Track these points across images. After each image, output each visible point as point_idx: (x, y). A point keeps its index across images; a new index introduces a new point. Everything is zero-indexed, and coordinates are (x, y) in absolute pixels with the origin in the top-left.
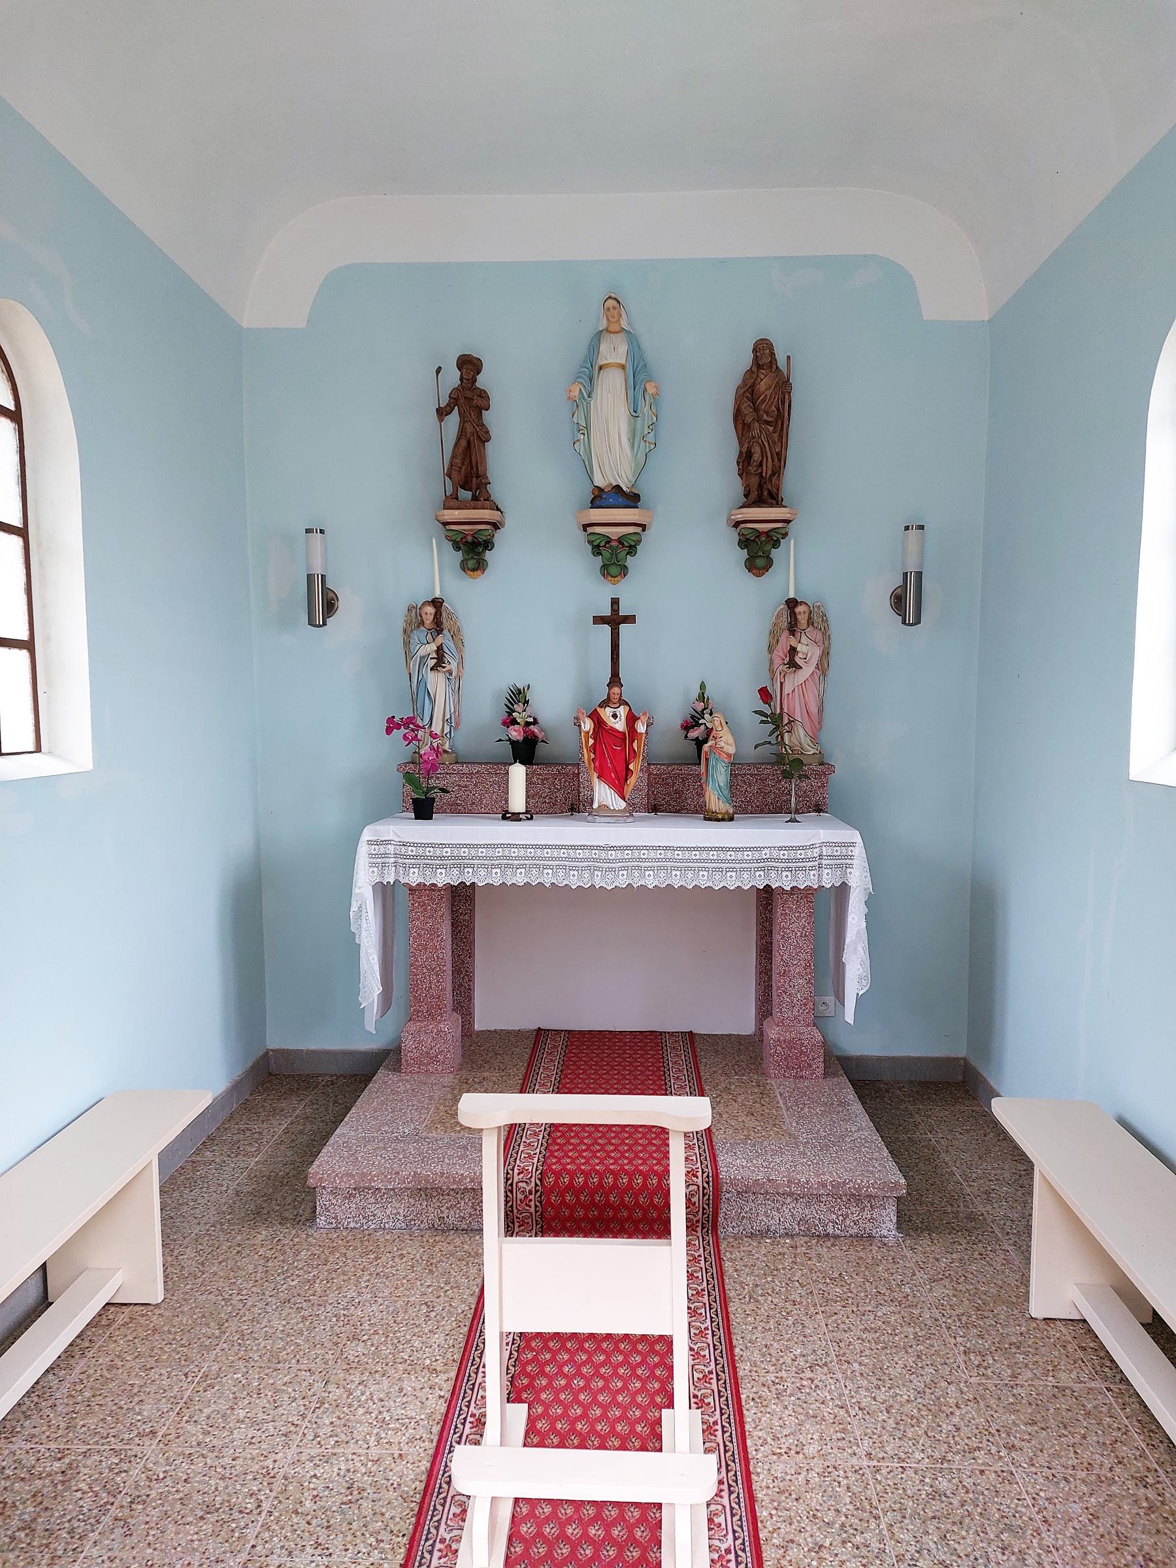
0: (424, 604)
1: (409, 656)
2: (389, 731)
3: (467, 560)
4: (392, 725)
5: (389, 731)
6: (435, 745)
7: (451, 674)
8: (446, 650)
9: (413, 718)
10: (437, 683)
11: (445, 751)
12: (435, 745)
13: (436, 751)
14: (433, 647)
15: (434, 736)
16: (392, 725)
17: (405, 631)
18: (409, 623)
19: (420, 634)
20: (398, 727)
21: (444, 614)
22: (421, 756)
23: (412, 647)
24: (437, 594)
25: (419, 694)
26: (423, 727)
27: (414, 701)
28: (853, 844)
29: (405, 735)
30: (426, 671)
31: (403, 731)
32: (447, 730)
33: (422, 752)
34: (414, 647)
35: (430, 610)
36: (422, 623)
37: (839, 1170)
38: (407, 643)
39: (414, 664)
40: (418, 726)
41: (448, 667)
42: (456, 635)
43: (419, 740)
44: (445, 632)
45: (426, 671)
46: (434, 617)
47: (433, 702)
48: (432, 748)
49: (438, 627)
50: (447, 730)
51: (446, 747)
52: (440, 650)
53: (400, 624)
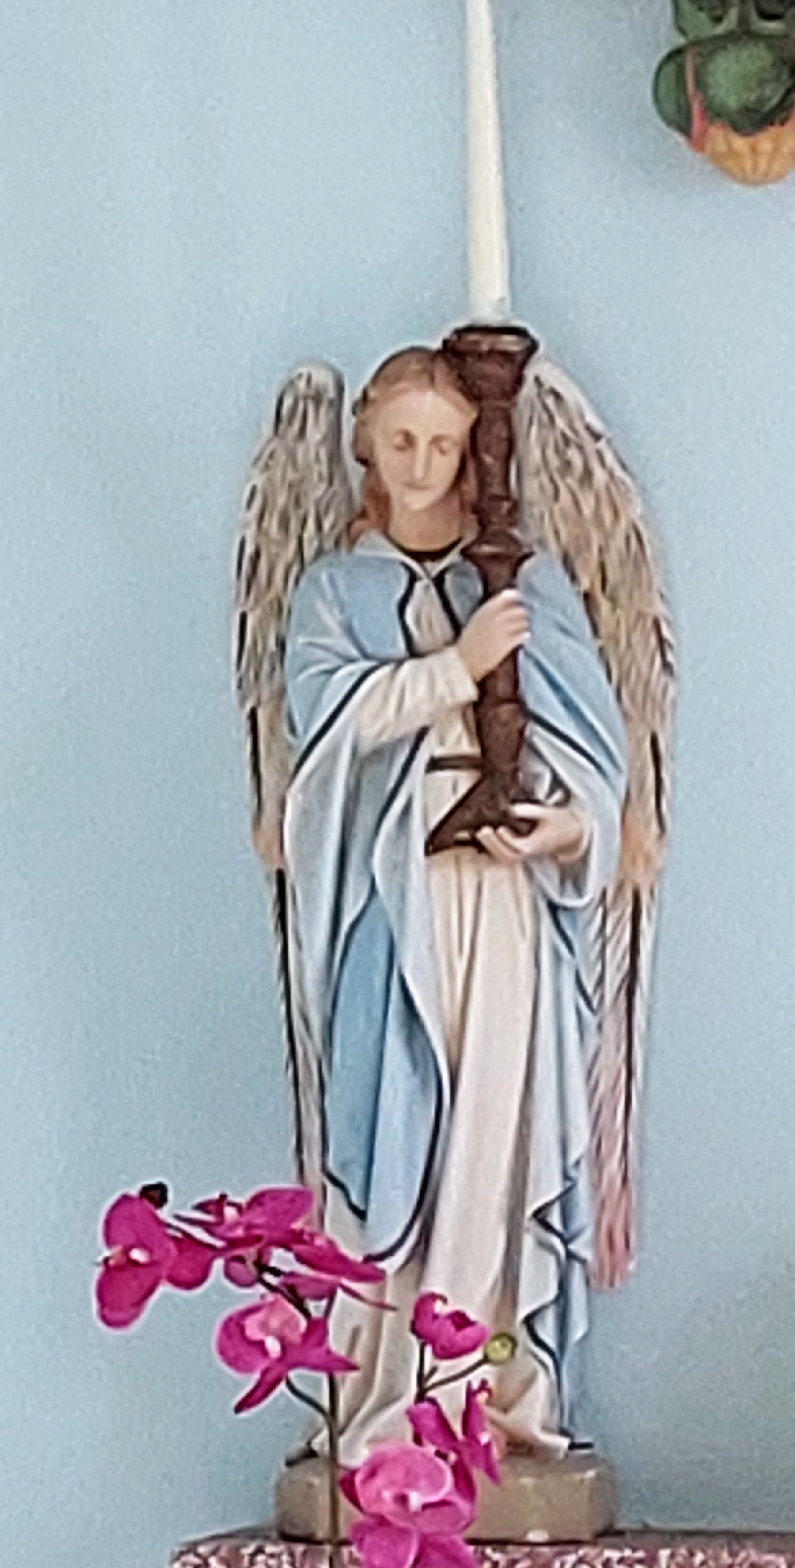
0: (389, 372)
1: (270, 741)
2: (120, 1294)
3: (707, 48)
4: (143, 1254)
5: (120, 1294)
6: (451, 1400)
7: (573, 875)
8: (538, 694)
9: (298, 1200)
10: (470, 939)
11: (521, 1448)
12: (451, 1400)
13: (459, 1444)
14: (451, 679)
15: (441, 1332)
16: (143, 1254)
17: (251, 567)
18: (276, 508)
19: (364, 588)
20: (188, 1265)
21: (533, 447)
22: (346, 1484)
23: (298, 686)
24: (489, 303)
25: (344, 1018)
26: (368, 1270)
27: (305, 1072)
28: (442, 743)
29: (234, 1328)
30: (399, 861)
31: (221, 1294)
32: (537, 1287)
33: (356, 1454)
34: (307, 694)
35: (436, 414)
36: (376, 507)
37: (438, 632)
38: (262, 659)
39: (311, 814)
40: (331, 1261)
41: (555, 826)
42: (613, 590)
43: (336, 1366)
44: (541, 570)
45: (399, 861)
46: (468, 464)
47: (441, 1091)
48: (428, 1423)
49: (486, 539)
50: (537, 1287)
51: (533, 1416)
52: (497, 700)
53: (217, 517)
